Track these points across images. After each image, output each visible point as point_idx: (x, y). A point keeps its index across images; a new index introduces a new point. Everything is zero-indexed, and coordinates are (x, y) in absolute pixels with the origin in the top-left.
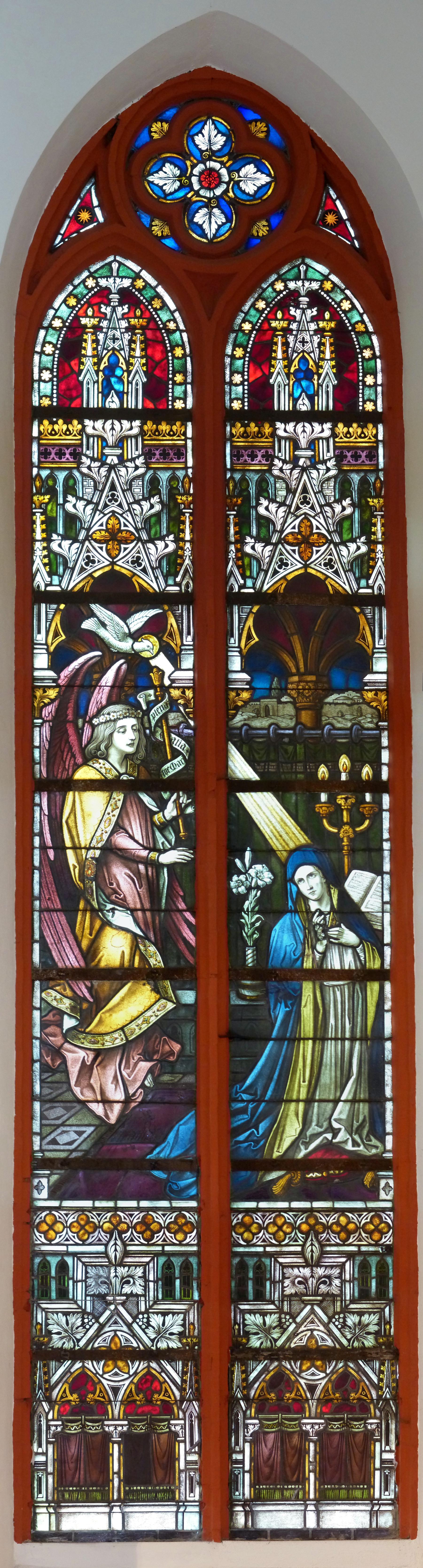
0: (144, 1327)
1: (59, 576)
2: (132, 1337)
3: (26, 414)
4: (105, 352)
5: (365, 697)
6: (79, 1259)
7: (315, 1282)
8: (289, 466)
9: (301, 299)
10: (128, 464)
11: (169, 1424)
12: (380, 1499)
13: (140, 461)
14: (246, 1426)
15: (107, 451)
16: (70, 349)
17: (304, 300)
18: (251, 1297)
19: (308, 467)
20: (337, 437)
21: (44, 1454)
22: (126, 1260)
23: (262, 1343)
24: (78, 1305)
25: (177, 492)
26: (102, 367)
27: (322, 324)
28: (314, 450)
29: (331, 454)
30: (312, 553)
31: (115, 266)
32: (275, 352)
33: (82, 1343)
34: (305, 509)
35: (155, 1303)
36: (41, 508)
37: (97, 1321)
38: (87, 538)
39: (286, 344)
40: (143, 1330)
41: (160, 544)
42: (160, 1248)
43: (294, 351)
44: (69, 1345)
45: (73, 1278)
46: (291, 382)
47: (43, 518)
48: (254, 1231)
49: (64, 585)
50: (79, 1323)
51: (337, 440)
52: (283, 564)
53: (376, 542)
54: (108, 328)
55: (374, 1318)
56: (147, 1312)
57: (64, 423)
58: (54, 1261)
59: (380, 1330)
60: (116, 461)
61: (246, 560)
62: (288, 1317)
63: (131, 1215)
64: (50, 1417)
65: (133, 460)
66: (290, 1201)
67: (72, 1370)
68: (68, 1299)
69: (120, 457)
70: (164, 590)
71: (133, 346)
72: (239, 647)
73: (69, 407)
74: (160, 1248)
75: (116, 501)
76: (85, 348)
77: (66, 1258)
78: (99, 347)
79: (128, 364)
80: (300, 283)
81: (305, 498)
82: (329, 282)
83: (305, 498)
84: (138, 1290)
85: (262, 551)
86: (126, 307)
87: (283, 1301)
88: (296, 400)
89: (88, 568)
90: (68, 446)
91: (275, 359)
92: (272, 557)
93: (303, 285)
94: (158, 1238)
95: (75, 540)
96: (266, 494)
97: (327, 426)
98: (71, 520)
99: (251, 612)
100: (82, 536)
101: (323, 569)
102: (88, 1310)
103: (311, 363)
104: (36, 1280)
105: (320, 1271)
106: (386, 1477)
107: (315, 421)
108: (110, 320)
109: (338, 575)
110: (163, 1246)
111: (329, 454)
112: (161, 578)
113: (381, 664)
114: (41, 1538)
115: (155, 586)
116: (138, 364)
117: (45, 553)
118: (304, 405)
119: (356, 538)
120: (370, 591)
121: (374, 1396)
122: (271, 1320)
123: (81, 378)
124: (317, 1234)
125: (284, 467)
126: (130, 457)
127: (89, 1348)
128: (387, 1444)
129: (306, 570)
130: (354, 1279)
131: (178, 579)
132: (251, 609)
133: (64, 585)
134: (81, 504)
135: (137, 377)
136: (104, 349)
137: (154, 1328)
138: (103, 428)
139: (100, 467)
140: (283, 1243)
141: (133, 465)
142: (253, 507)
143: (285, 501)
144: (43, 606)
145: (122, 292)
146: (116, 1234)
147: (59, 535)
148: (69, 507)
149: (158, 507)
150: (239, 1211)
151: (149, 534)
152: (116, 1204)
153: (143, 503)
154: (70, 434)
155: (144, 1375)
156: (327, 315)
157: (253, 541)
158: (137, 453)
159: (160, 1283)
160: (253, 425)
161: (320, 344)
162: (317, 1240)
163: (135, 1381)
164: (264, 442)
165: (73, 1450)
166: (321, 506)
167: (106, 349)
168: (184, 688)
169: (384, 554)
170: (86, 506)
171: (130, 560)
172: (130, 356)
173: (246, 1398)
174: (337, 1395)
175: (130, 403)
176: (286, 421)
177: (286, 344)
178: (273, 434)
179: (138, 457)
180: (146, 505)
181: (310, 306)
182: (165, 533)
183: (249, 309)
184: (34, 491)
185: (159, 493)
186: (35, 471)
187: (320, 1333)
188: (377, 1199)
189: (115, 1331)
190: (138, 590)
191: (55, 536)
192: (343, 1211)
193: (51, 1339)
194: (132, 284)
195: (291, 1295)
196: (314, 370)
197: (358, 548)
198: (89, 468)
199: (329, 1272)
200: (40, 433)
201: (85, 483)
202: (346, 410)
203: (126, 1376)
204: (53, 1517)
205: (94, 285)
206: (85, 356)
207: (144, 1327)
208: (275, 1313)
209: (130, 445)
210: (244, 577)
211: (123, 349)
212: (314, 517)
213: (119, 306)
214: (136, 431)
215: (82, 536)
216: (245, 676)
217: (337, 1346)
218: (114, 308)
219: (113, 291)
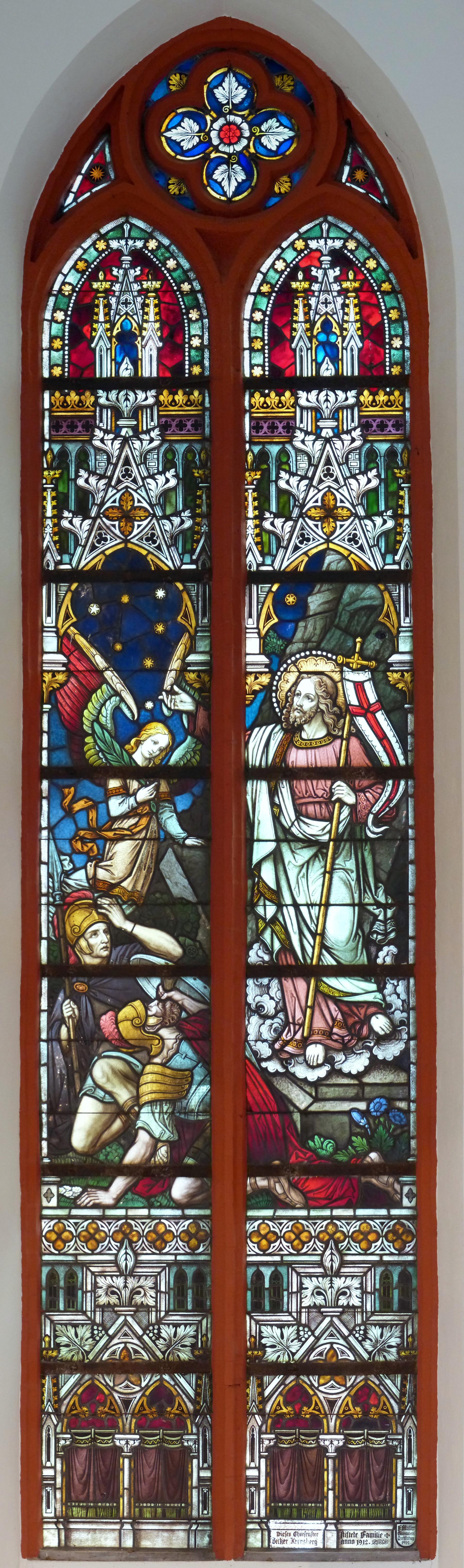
0: (360, 1339)
1: (70, 554)
2: (349, 1349)
3: (32, 383)
4: (118, 317)
5: (187, 679)
6: (293, 1269)
7: (334, 1293)
8: (111, 436)
9: (124, 258)
10: (143, 436)
11: (182, 1439)
12: (402, 1518)
13: (356, 433)
14: (261, 1441)
15: (321, 424)
16: (82, 314)
17: (326, 259)
18: (267, 1308)
19: (130, 437)
20: (161, 405)
21: (52, 1468)
22: (343, 1270)
23: (279, 1357)
24: (87, 1316)
25: (193, 465)
26: (115, 332)
27: (346, 285)
28: (337, 420)
29: (155, 422)
30: (133, 527)
31: (126, 227)
32: (97, 314)
33: (91, 1356)
34: (127, 483)
35: (167, 1312)
36: (52, 483)
37: (313, 1334)
38: (301, 515)
39: (108, 306)
40: (154, 1342)
41: (378, 520)
42: (173, 1258)
43: (116, 313)
44: (284, 1359)
45: (82, 1289)
46: (114, 346)
47: (54, 494)
48: (304, 1239)
49: (277, 565)
50: (88, 1335)
51: (161, 408)
52: (304, 539)
53: (403, 516)
54: (320, 291)
55: (191, 1330)
56: (364, 1323)
57: (92, 395)
58: (267, 1272)
59: (403, 1342)
60: (331, 434)
61: (265, 537)
62: (100, 1328)
63: (281, 1224)
64: (58, 1430)
65: (348, 432)
66: (355, 1208)
67: (82, 1382)
68: (283, 1312)
69: (135, 429)
70: (382, 569)
71: (346, 310)
72: (258, 628)
73: (81, 377)
74: (173, 1258)
75: (130, 476)
76: (296, 314)
77: (280, 1269)
78: (311, 312)
79: (342, 329)
80: (123, 242)
81: (127, 470)
82: (154, 241)
83: (328, 470)
84: (355, 1301)
85: (81, 526)
86: (337, 269)
87: (95, 1312)
88: (319, 365)
89: (303, 546)
90: (281, 419)
91: (97, 322)
92: (292, 533)
93: (127, 244)
94: (376, 1247)
95: (289, 518)
96: (85, 466)
97: (352, 394)
98: (84, 495)
99: (270, 590)
100: (295, 513)
101: (346, 545)
102: (303, 1321)
103: (135, 325)
104: (47, 1290)
105: (339, 1283)
106: (409, 1496)
107: (138, 389)
108: (122, 283)
109: (364, 551)
110: (381, 1256)
111: (152, 424)
112: (176, 556)
113: (405, 645)
114: (52, 1555)
115: (170, 564)
116: (353, 329)
117: (257, 531)
118: (327, 370)
119: (382, 512)
120: (396, 567)
121: (397, 1411)
122: (289, 1332)
123: (93, 345)
124: (337, 1242)
125: (106, 438)
126: (145, 428)
127: (305, 1361)
128: (410, 1461)
129: (126, 545)
130: (375, 1289)
131: (397, 558)
132: (271, 588)
133: (277, 565)
134: (294, 481)
135: (352, 342)
136: (317, 313)
137: (371, 1340)
138: (117, 398)
139: (314, 441)
140: (164, 1251)
141: (148, 437)
142: (72, 480)
143: (306, 474)
144: (254, 588)
145: (333, 253)
146: (331, 1242)
147: (271, 513)
148: (81, 482)
149: (173, 482)
150: (256, 1219)
151: (164, 511)
152: (389, 1212)
153: (359, 477)
154: (376, 405)
155: (157, 1387)
156: (351, 275)
157: (71, 515)
158: (353, 425)
159: (172, 1293)
160: (73, 394)
161: (344, 306)
162: (132, 1249)
163: (147, 1393)
164: (284, 412)
165: (79, 1465)
166: (143, 479)
167: (119, 314)
168: (402, 671)
169: (411, 527)
170: (300, 481)
171: (346, 538)
172: (343, 321)
173: (57, 1412)
174: (85, 1409)
175: (347, 371)
176: (108, 390)
177: (108, 306)
178: (96, 404)
179: (355, 429)
180: (363, 479)
181: (333, 266)
182: (181, 508)
183: (268, 270)
184: (45, 466)
185: (174, 466)
186: (46, 446)
187: (340, 1344)
188: (399, 1205)
189: (332, 1344)
190: (355, 569)
191: (267, 515)
192: (364, 1219)
193: (265, 1352)
194: (344, 244)
195: (309, 1307)
196: (137, 333)
197: (182, 522)
198: (102, 441)
199: (349, 1282)
200: (51, 405)
201: (98, 457)
202: (371, 377)
203: (137, 1388)
204: (63, 1534)
205: (105, 248)
206: (296, 322)
207: (154, 1338)
208: (293, 1325)
209: (346, 414)
210: (262, 554)
211: (336, 313)
212: (135, 491)
213: (131, 268)
214: (151, 401)
215: (295, 513)
216: (61, 658)
217: (152, 1359)
218: (126, 270)
219: (126, 253)
